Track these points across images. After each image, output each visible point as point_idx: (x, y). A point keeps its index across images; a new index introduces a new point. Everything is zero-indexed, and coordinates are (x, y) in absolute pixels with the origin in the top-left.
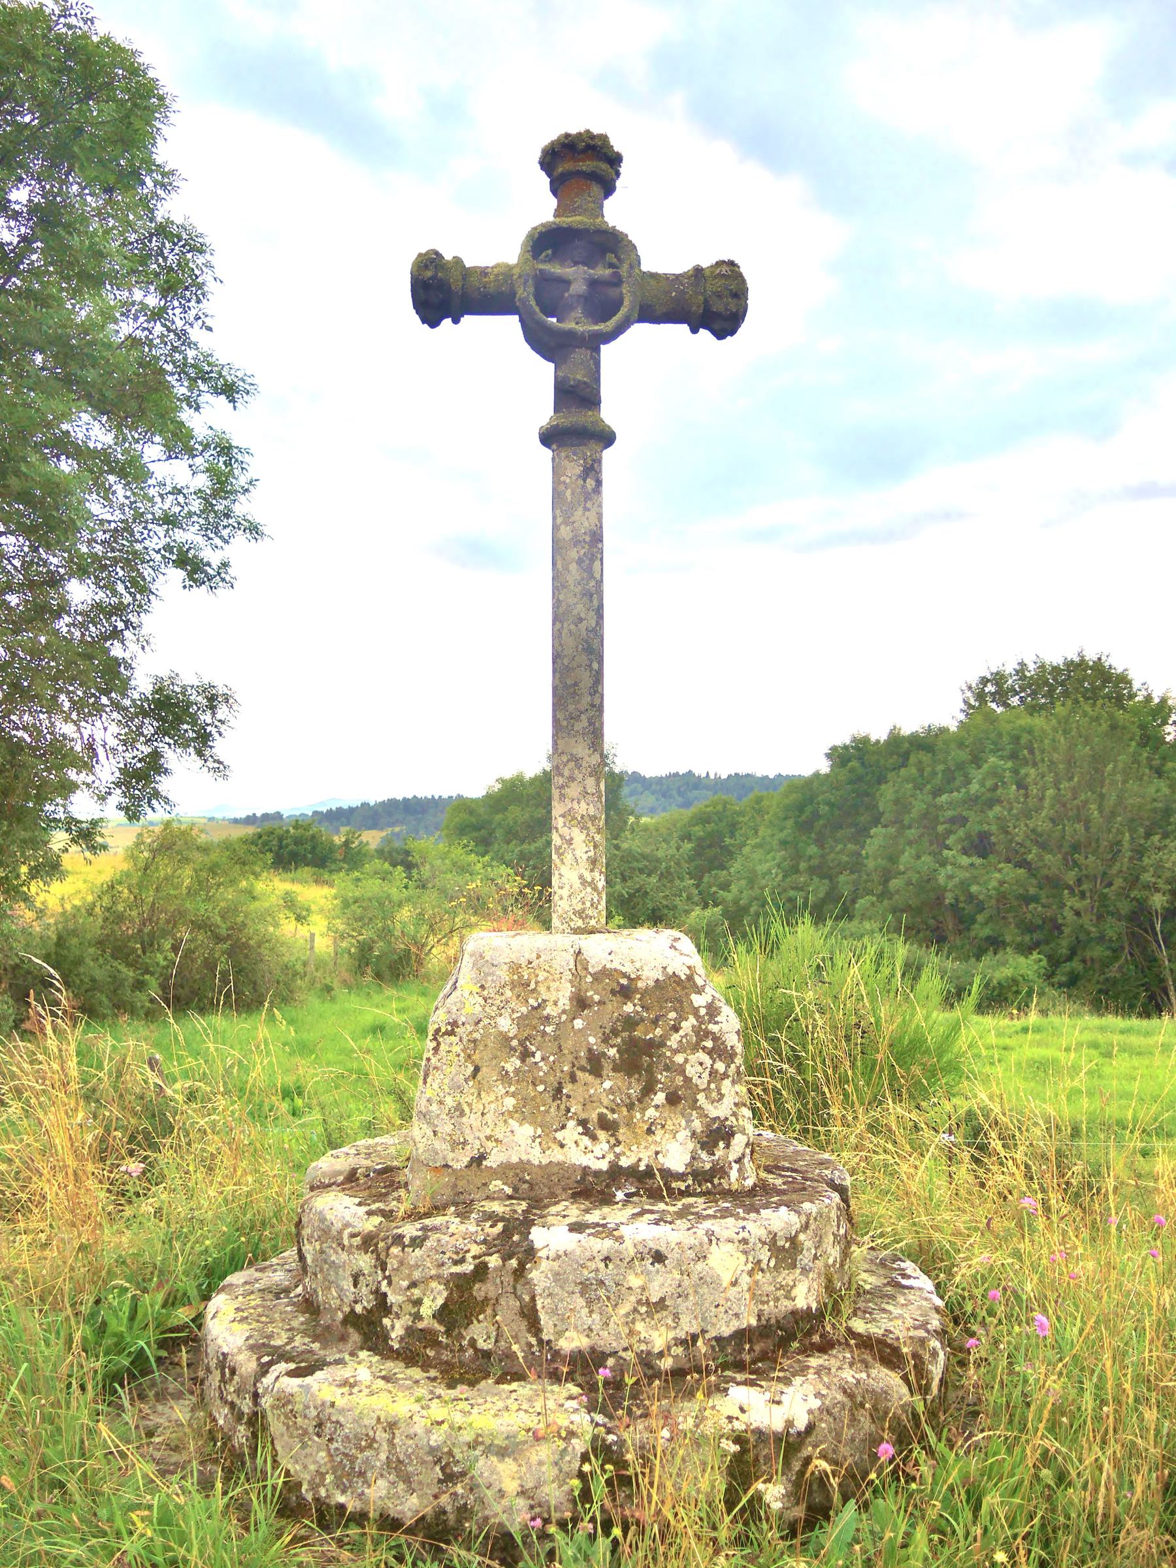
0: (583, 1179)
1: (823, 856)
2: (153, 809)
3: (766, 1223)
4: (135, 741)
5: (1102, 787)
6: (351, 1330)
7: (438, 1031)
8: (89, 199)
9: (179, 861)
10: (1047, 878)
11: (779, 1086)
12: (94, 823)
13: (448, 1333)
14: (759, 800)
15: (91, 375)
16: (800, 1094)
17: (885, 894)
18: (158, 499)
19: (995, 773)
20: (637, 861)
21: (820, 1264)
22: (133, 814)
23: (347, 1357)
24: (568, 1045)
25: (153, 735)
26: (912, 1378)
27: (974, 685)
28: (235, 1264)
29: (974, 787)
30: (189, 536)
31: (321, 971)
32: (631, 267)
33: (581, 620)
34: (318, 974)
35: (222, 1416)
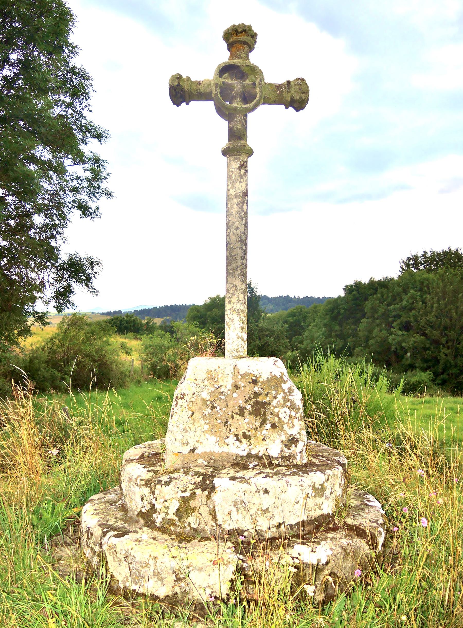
0: (236, 458)
1: (341, 331)
2: (68, 308)
3: (311, 478)
4: (60, 280)
5: (457, 303)
6: (140, 519)
7: (177, 397)
8: (42, 57)
9: (79, 329)
10: (434, 340)
11: (319, 422)
12: (44, 313)
13: (179, 521)
14: (315, 307)
15: (43, 130)
16: (327, 426)
17: (367, 346)
18: (70, 181)
19: (413, 297)
20: (265, 331)
21: (333, 496)
22: (59, 310)
23: (138, 530)
24: (231, 403)
25: (68, 278)
26: (370, 543)
27: (405, 261)
28: (96, 491)
29: (404, 303)
30: (83, 196)
31: (136, 374)
32: (261, 81)
33: (238, 228)
34: (135, 376)
35: (88, 552)
